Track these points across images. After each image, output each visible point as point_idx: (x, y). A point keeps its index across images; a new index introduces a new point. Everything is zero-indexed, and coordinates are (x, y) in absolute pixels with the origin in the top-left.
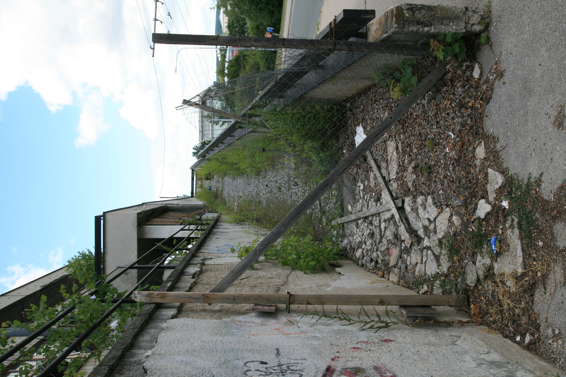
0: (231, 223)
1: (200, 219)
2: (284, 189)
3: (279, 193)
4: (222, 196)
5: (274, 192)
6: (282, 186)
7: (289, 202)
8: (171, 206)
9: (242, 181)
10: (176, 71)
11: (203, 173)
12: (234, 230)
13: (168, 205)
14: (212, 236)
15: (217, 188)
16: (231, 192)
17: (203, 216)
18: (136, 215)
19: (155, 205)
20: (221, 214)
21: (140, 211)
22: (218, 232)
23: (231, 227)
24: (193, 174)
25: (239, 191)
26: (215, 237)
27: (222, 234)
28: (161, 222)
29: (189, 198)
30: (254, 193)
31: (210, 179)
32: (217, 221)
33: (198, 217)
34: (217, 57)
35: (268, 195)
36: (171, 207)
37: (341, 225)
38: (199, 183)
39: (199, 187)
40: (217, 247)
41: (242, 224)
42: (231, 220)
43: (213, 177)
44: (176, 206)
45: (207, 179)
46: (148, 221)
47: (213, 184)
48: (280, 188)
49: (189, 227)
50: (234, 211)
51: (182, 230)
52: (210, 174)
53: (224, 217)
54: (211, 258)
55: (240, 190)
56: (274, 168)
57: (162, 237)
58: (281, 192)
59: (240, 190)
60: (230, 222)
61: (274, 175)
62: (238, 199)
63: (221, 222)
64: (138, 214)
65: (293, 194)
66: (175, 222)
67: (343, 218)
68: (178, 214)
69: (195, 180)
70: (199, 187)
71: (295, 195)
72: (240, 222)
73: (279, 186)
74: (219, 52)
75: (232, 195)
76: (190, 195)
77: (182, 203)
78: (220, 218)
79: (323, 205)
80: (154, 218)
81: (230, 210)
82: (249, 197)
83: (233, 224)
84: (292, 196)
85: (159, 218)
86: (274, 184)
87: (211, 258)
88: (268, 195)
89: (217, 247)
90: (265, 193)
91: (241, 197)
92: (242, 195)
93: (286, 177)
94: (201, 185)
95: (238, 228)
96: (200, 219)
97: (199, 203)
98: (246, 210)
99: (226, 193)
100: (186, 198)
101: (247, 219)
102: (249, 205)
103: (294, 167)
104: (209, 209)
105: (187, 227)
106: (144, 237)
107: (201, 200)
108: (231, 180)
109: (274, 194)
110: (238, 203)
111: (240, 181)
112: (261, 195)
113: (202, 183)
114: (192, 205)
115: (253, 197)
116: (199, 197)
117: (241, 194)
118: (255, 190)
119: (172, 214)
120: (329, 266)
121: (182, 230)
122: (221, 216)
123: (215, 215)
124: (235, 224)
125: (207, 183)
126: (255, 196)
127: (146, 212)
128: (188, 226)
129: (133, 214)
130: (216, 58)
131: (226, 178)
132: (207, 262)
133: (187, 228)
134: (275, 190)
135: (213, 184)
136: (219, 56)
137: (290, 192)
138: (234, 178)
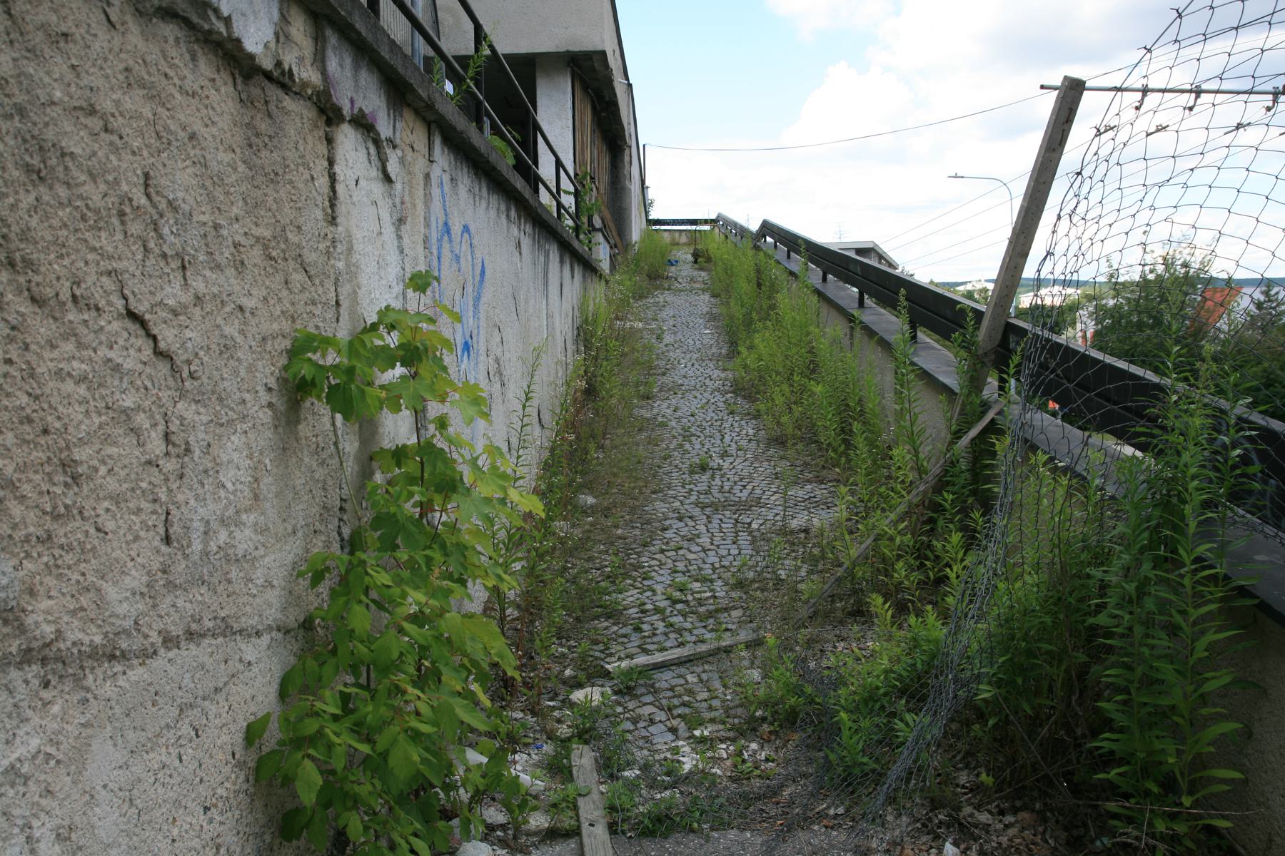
0: (583, 307)
1: (593, 229)
2: (703, 487)
3: (685, 467)
4: (656, 289)
5: (687, 446)
6: (713, 478)
7: (661, 507)
8: (626, 159)
9: (706, 340)
10: (956, 177)
11: (715, 244)
12: (557, 315)
13: (627, 152)
14: (529, 228)
15: (676, 279)
16: (668, 312)
17: (600, 235)
18: (600, 48)
19: (628, 116)
20: (607, 282)
21: (613, 62)
22: (547, 256)
23: (567, 307)
24: (706, 222)
25: (675, 333)
26: (526, 242)
27: (541, 275)
28: (582, 122)
29: (647, 213)
30: (676, 377)
31: (696, 262)
32: (588, 267)
33: (597, 222)
34: (965, 283)
35: (673, 423)
36: (622, 161)
37: (567, 822)
38: (684, 239)
39: (673, 239)
40: (466, 229)
41: (576, 342)
42: (591, 307)
43: (701, 269)
44: (626, 173)
45: (696, 256)
46: (586, 87)
47: (684, 268)
48: (703, 468)
49: (569, 193)
50: (617, 318)
51: (559, 164)
52: (709, 260)
53: (598, 291)
54: (387, 179)
55: (680, 336)
56: (768, 446)
57: (539, 104)
58: (692, 473)
59: (680, 336)
60: (582, 304)
61: (744, 443)
62: (652, 331)
63: (584, 276)
64: (603, 54)
65: (691, 523)
66: (583, 163)
67: (601, 831)
68: (604, 178)
69: (689, 228)
70: (673, 239)
71: (685, 531)
72: (584, 334)
73: (711, 464)
74: (979, 286)
75: (664, 315)
76: (650, 218)
77: (632, 188)
78: (596, 279)
79: (665, 679)
80: (594, 108)
81: (621, 309)
82: (662, 363)
83: (577, 313)
84: (680, 519)
85: (593, 120)
86: (714, 446)
87: (387, 179)
88: (673, 423)
89: (466, 229)
90: (679, 413)
91: (659, 338)
92: (665, 341)
93: (745, 493)
94: (678, 244)
95: (563, 328)
96: (593, 229)
97: (636, 231)
98: (623, 355)
99: (667, 299)
100: (646, 205)
101: (596, 358)
102: (636, 363)
103: (794, 524)
104: (619, 258)
105: (566, 184)
106: (538, 74)
107: (643, 240)
108: (705, 310)
109: (681, 446)
110: (640, 331)
111: (707, 335)
112: (674, 402)
113: (684, 244)
114: (630, 214)
115: (664, 374)
116: (647, 236)
117: (668, 338)
118: (686, 382)
119: (606, 161)
120: (332, 833)
121: (559, 164)
122: (603, 282)
123: (605, 266)
124: (578, 322)
125: (685, 255)
126: (667, 380)
127: (609, 82)
128: (572, 189)
129: (603, 41)
130: (960, 281)
131: (707, 297)
132: (348, 141)
133: (563, 186)
134: (696, 450)
135: (684, 268)
136: (969, 287)
137: (696, 512)
138: (712, 318)
